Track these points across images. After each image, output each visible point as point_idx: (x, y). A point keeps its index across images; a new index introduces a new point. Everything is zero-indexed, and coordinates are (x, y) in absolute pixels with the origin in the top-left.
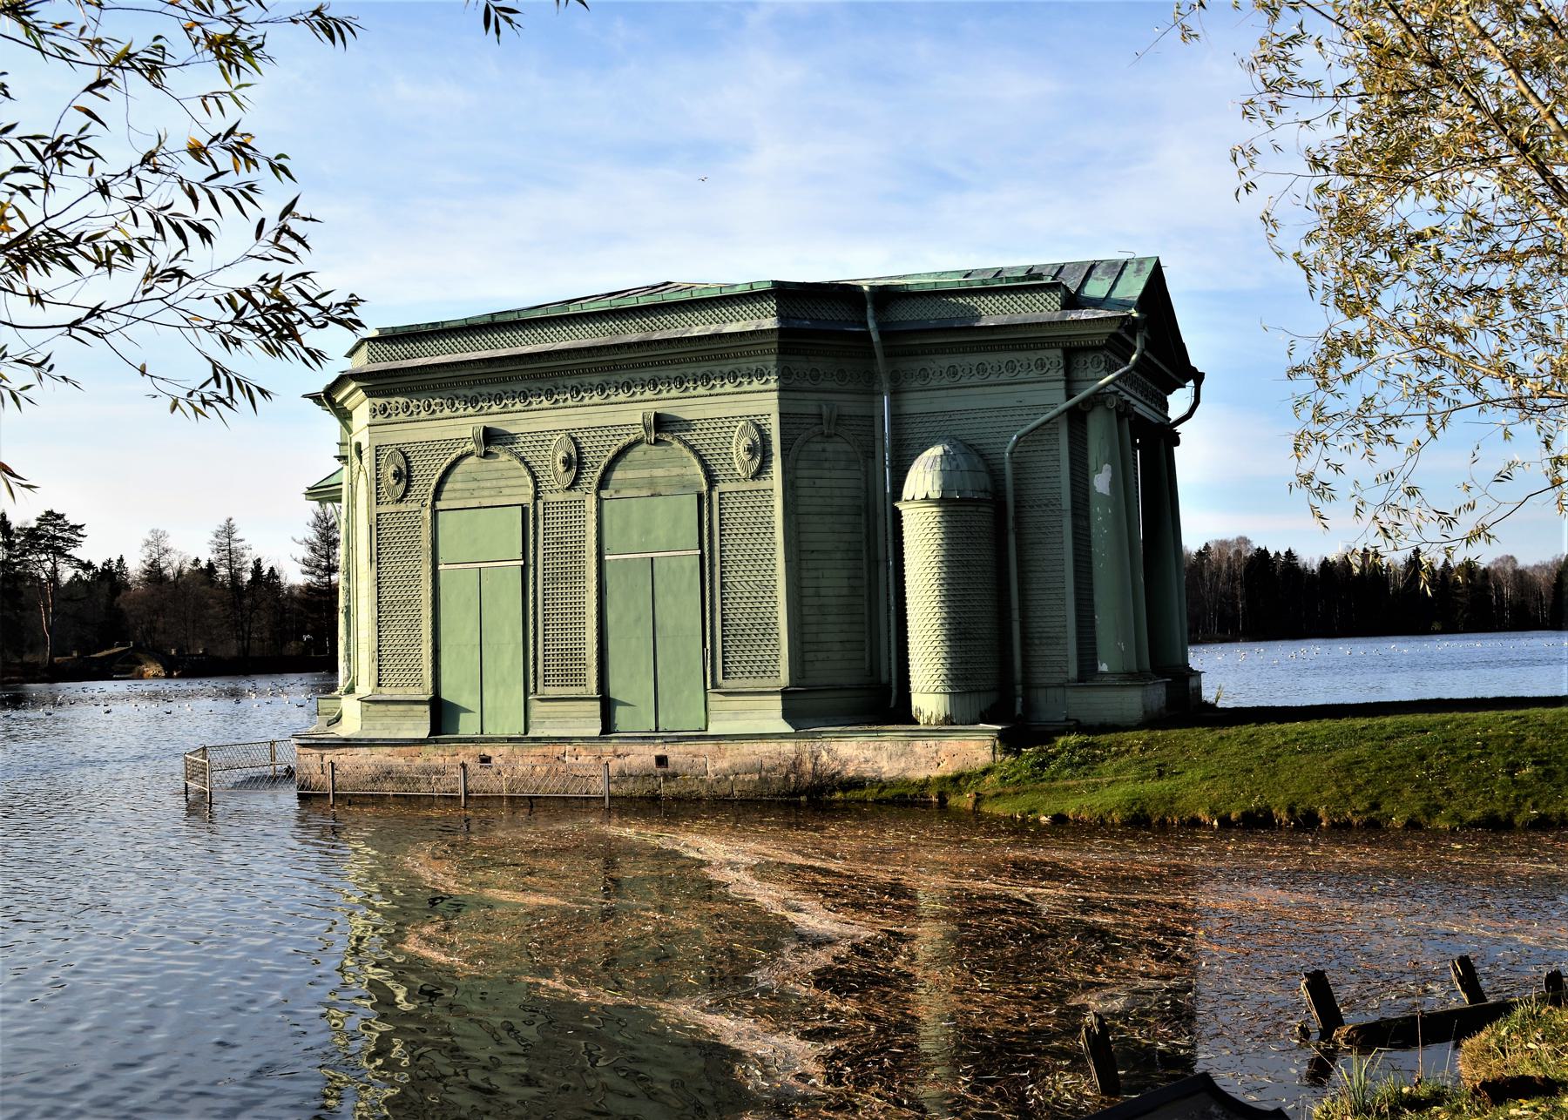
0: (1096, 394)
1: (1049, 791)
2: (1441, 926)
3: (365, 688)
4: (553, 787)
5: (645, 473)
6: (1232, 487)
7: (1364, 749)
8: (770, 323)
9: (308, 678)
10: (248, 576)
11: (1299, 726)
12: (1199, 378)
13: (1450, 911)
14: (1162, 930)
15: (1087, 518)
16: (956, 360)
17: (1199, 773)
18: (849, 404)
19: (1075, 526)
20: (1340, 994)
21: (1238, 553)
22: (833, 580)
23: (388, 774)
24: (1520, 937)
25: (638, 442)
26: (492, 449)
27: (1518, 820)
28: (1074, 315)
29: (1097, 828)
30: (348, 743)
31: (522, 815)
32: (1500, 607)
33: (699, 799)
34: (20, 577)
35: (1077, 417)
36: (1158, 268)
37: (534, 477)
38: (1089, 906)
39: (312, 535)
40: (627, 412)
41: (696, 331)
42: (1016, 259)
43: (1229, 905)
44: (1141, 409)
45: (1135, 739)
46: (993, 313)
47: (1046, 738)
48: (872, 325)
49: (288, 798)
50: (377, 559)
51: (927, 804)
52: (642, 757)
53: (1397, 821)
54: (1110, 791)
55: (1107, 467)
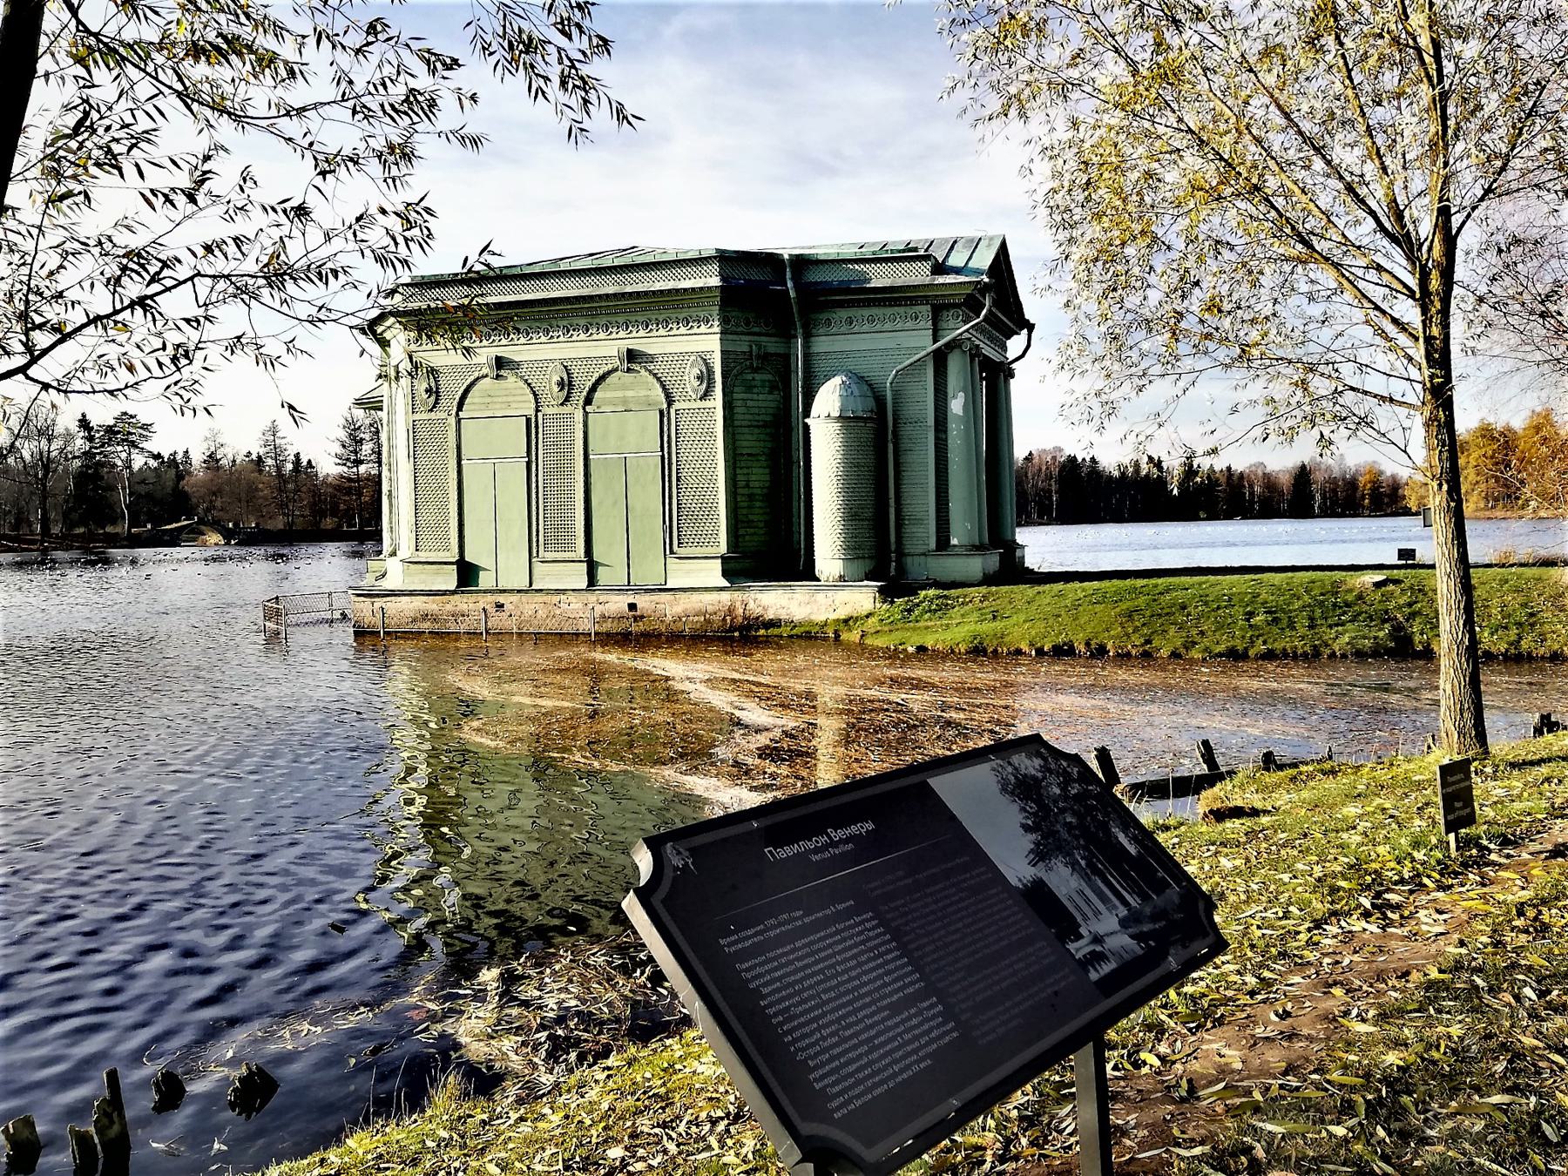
0: (954, 340)
1: (914, 629)
2: (1194, 722)
3: (406, 551)
4: (552, 626)
5: (620, 394)
6: (1050, 415)
7: (1141, 601)
8: (715, 281)
9: (344, 546)
10: (289, 466)
11: (1096, 584)
12: (1031, 327)
13: (1200, 712)
14: (998, 723)
15: (946, 432)
16: (852, 312)
17: (1022, 617)
18: (772, 345)
19: (937, 438)
20: (1119, 766)
21: (1054, 458)
22: (759, 476)
23: (425, 617)
24: (1249, 730)
25: (616, 370)
26: (502, 372)
27: (1251, 653)
28: (941, 280)
29: (949, 655)
30: (393, 594)
31: (529, 645)
32: (1252, 502)
33: (660, 635)
34: (100, 464)
35: (940, 359)
36: (1003, 246)
37: (535, 395)
38: (945, 707)
39: (343, 435)
40: (605, 346)
41: (658, 286)
42: (897, 235)
43: (1045, 707)
44: (987, 351)
45: (976, 592)
46: (880, 277)
47: (911, 590)
48: (790, 284)
49: (346, 634)
50: (414, 456)
51: (826, 639)
52: (618, 604)
53: (1164, 653)
54: (959, 627)
55: (961, 394)
